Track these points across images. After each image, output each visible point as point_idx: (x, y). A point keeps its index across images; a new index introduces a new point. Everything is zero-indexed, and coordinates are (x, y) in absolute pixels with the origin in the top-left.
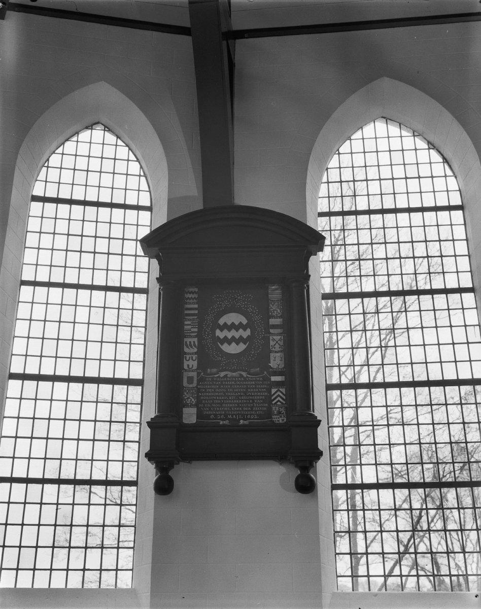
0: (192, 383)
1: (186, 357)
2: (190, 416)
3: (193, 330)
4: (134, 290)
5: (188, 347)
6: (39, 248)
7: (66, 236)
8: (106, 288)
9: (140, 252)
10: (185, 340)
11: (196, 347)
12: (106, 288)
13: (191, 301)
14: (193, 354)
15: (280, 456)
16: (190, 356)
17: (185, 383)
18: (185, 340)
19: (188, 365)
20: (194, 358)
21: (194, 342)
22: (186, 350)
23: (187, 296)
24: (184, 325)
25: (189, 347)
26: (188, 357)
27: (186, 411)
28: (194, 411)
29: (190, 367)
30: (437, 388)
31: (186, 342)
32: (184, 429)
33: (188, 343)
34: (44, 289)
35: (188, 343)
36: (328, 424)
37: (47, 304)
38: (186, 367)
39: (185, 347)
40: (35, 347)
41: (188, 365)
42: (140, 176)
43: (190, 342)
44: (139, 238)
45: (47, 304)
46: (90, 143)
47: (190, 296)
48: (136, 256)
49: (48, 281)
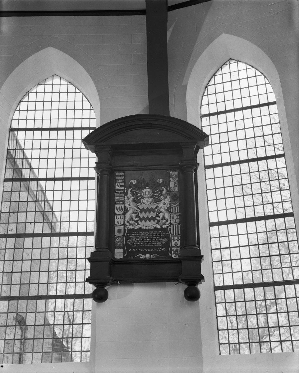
0: (118, 230)
1: (116, 217)
2: (119, 254)
3: (120, 199)
4: (213, 166)
5: (117, 210)
6: (225, 198)
7: (71, 159)
8: (80, 179)
9: (83, 146)
10: (116, 206)
11: (122, 210)
12: (80, 179)
13: (120, 181)
14: (121, 214)
15: (174, 279)
16: (120, 216)
17: (116, 233)
18: (116, 206)
19: (118, 222)
20: (122, 218)
21: (122, 207)
22: (117, 212)
23: (117, 178)
24: (115, 196)
25: (119, 210)
26: (118, 217)
27: (116, 251)
28: (121, 251)
29: (119, 223)
30: (269, 214)
31: (117, 207)
32: (115, 262)
33: (118, 208)
34: (233, 160)
35: (118, 208)
36: (212, 261)
37: (62, 190)
38: (116, 223)
39: (116, 210)
40: (83, 195)
41: (118, 222)
42: (90, 110)
43: (119, 207)
44: (83, 138)
45: (62, 190)
46: (74, 110)
47: (120, 178)
48: (81, 148)
49: (214, 168)
